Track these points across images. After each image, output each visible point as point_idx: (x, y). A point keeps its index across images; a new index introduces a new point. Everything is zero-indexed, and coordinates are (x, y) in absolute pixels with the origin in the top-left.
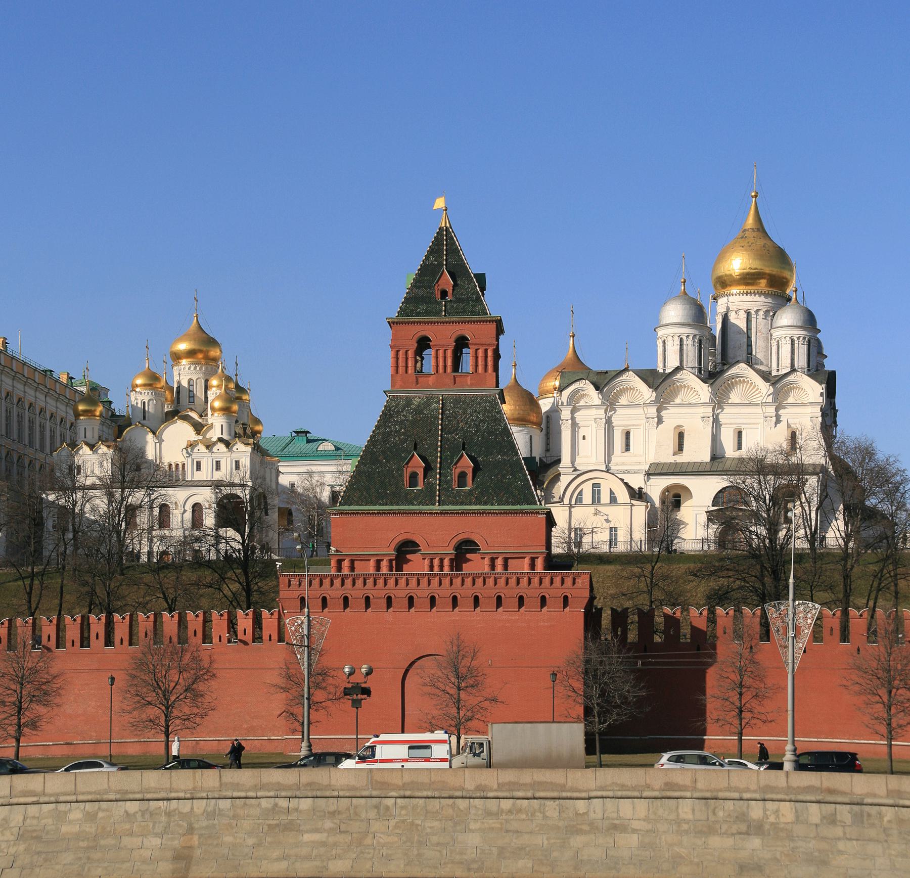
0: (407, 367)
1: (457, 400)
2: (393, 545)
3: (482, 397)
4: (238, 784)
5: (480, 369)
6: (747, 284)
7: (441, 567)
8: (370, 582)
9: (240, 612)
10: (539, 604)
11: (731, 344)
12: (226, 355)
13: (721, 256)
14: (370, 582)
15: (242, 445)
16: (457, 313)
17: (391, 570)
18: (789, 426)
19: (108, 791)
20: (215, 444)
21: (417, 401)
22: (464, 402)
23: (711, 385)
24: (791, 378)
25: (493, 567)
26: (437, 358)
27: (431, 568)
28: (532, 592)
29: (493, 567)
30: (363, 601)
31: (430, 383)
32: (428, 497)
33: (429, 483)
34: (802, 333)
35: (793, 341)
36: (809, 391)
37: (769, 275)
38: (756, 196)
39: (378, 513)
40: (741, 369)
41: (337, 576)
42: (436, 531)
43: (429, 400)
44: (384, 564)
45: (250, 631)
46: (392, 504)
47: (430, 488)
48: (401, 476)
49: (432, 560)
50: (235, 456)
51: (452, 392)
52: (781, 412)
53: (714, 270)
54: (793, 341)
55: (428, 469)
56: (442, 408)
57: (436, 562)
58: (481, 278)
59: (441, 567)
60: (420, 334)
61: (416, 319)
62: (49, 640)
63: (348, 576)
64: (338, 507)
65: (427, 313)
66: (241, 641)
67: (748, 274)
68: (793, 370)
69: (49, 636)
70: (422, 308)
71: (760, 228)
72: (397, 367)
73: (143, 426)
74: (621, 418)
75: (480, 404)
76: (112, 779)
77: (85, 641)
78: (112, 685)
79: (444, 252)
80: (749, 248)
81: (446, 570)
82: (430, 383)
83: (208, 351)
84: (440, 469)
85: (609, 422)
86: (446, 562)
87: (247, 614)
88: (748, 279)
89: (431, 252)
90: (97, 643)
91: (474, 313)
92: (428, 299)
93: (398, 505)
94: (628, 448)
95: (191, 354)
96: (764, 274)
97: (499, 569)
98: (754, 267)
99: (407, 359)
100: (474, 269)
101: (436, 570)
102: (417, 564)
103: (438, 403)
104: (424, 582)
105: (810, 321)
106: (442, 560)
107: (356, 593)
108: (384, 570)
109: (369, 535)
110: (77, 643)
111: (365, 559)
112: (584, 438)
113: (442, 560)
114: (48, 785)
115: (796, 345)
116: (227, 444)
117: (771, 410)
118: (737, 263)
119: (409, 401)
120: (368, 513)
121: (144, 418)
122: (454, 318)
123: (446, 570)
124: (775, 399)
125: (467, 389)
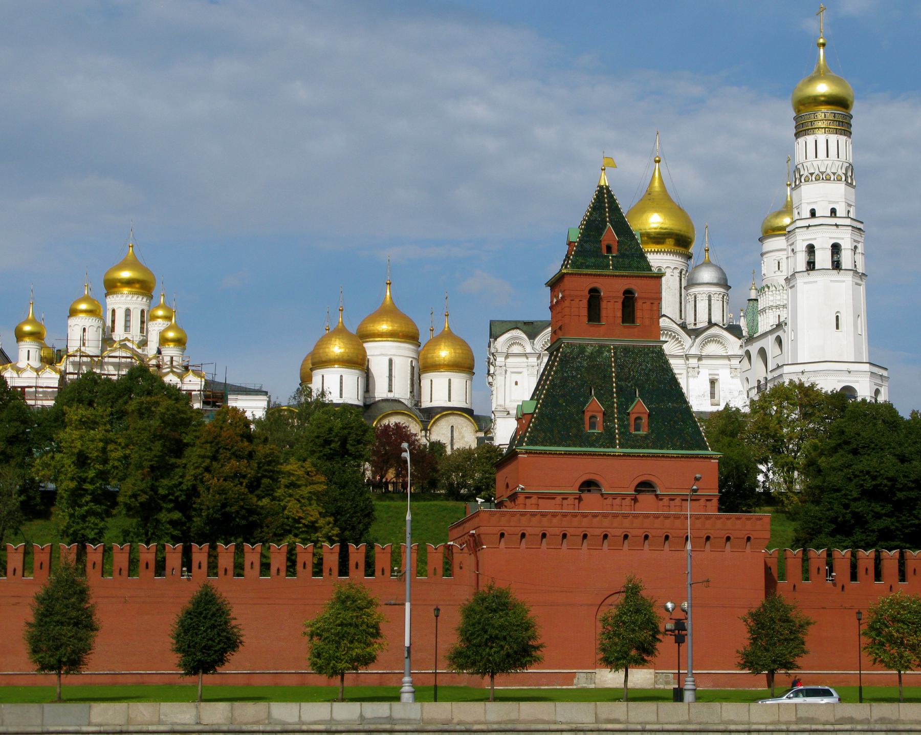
1: (626, 350)
4: (813, 719)
9: (195, 547)
16: (625, 268)
19: (689, 722)
21: (589, 350)
32: (608, 439)
33: (607, 426)
39: (624, 456)
42: (618, 470)
46: (575, 445)
47: (609, 432)
48: (582, 419)
54: (710, 297)
61: (589, 271)
64: (525, 446)
65: (597, 266)
68: (711, 324)
75: (648, 354)
76: (692, 710)
79: (605, 210)
90: (252, 573)
91: (638, 268)
92: (597, 254)
93: (581, 446)
98: (665, 226)
103: (609, 351)
114: (632, 714)
119: (582, 349)
120: (639, 456)
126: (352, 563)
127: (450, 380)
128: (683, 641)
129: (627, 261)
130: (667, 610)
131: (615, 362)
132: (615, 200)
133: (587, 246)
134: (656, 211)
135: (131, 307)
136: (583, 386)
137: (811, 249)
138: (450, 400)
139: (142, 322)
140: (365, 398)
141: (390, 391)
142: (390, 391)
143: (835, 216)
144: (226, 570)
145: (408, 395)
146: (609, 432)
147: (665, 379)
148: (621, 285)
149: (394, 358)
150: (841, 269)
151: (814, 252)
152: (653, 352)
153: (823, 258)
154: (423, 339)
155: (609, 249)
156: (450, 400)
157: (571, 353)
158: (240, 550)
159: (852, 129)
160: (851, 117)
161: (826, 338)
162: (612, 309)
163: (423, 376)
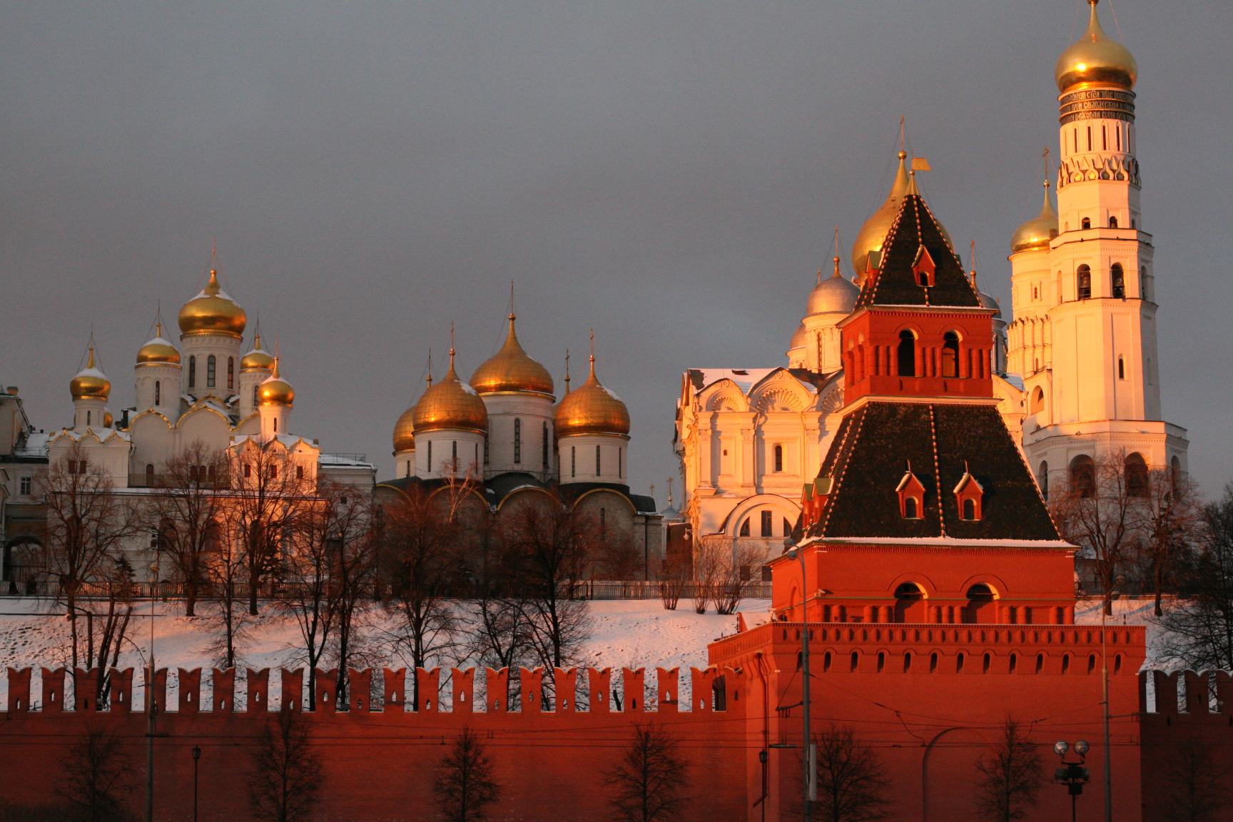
0: (889, 367)
2: (893, 589)
7: (951, 619)
10: (849, 664)
25: (1013, 618)
27: (939, 619)
29: (1013, 618)
31: (917, 388)
38: (904, 157)
44: (882, 612)
49: (939, 609)
55: (928, 498)
56: (934, 420)
57: (945, 611)
58: (958, 258)
59: (951, 619)
72: (877, 366)
74: (775, 429)
78: (196, 759)
82: (917, 388)
84: (942, 494)
85: (758, 432)
86: (957, 611)
94: (779, 466)
101: (945, 622)
102: (922, 615)
112: (725, 453)
113: (951, 609)
123: (957, 622)
127: (598, 447)
128: (1080, 792)
131: (936, 427)
132: (928, 215)
135: (216, 354)
137: (1084, 272)
138: (598, 474)
139: (231, 372)
141: (517, 462)
142: (517, 462)
143: (1116, 227)
145: (541, 468)
149: (522, 418)
150: (1124, 298)
151: (1089, 276)
153: (1100, 283)
154: (559, 393)
156: (598, 474)
159: (1136, 112)
160: (1134, 96)
163: (561, 441)
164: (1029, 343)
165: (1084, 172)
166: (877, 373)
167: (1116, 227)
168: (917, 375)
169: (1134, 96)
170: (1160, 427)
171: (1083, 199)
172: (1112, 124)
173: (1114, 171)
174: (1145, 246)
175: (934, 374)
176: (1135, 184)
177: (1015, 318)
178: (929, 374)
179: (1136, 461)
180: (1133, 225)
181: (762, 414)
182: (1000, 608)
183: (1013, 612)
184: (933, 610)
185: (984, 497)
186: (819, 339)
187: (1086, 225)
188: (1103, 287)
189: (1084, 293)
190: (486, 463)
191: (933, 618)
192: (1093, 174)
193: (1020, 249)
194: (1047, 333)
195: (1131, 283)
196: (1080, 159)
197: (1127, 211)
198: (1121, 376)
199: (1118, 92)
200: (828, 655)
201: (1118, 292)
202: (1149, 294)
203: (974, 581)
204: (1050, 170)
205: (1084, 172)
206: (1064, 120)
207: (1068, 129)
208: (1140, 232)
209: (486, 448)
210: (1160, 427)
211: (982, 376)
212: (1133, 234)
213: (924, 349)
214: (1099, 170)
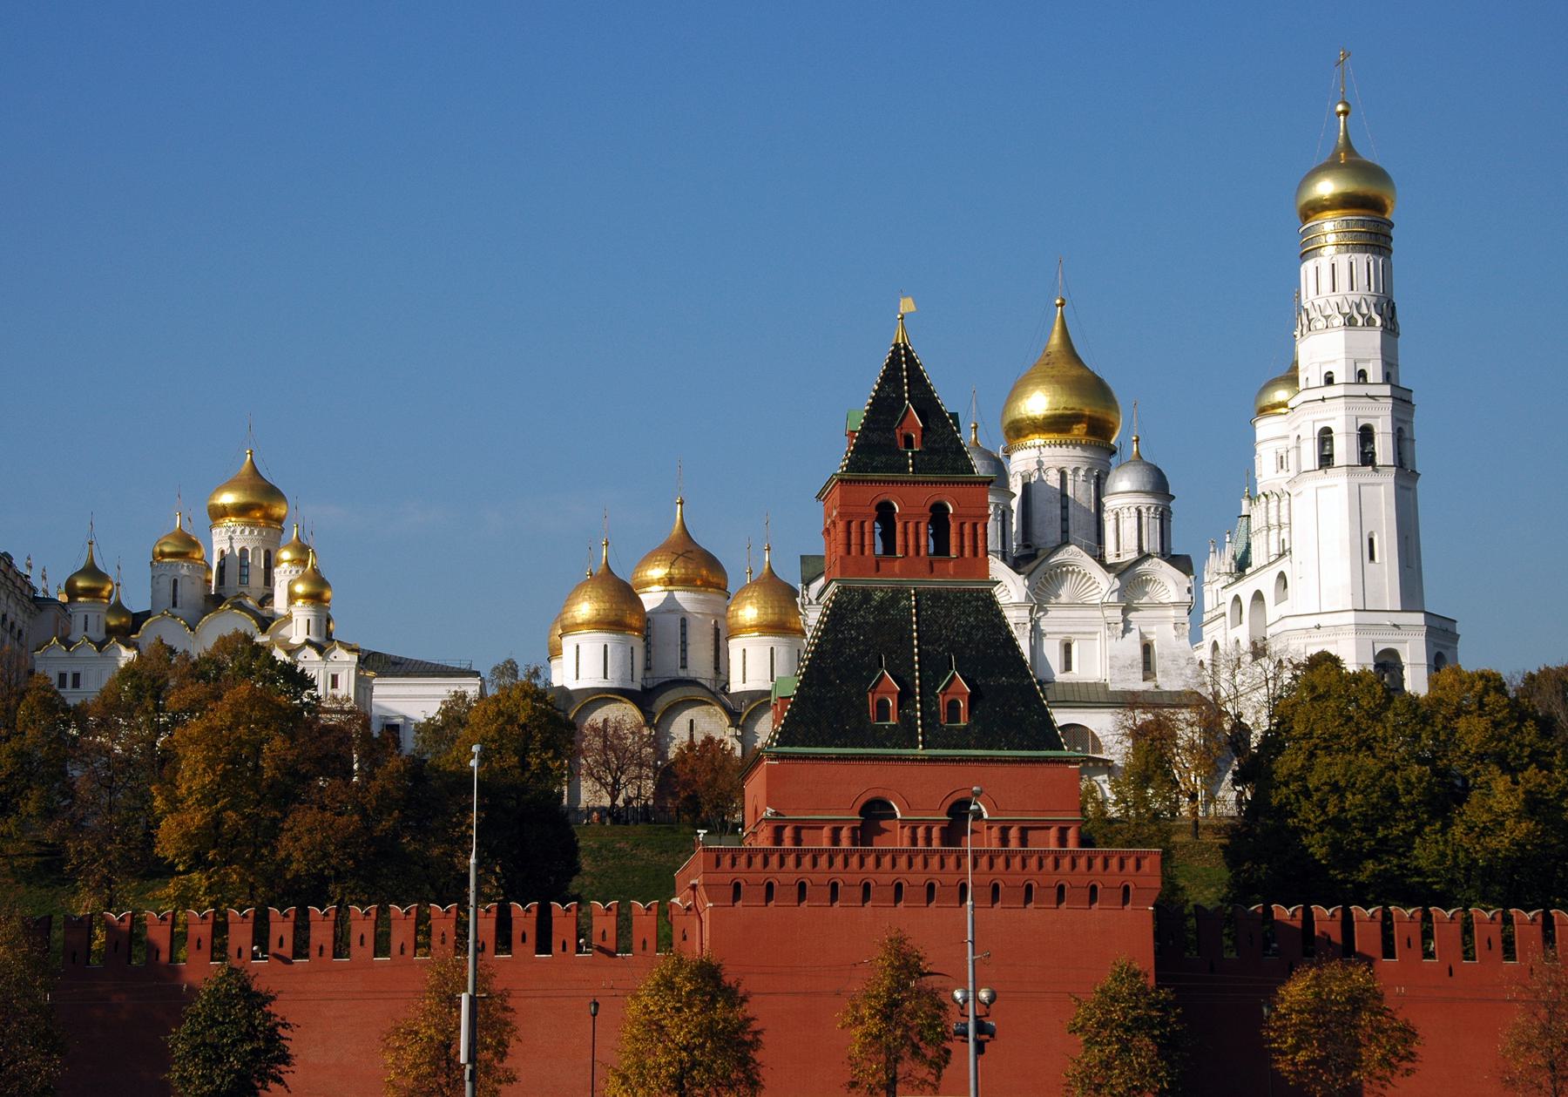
0: (863, 546)
1: (936, 596)
3: (971, 591)
5: (967, 552)
6: (1060, 431)
7: (928, 841)
8: (903, 862)
9: (517, 907)
10: (1055, 898)
11: (1036, 517)
12: (296, 513)
13: (1016, 391)
14: (903, 862)
15: (344, 652)
16: (932, 471)
17: (854, 844)
18: (1142, 636)
20: (301, 647)
22: (947, 599)
23: (1028, 576)
24: (1145, 567)
25: (1004, 840)
26: (849, 533)
27: (914, 841)
28: (1074, 880)
29: (1004, 840)
30: (828, 889)
31: (897, 569)
34: (1149, 501)
35: (1140, 513)
36: (1011, 587)
37: (1090, 418)
38: (1062, 305)
40: (1073, 554)
41: (772, 852)
42: (916, 786)
43: (898, 594)
44: (845, 833)
45: (611, 934)
47: (907, 721)
49: (914, 830)
50: (332, 668)
51: (936, 583)
52: (1132, 616)
53: (1004, 414)
54: (1140, 513)
55: (905, 697)
57: (921, 832)
58: (954, 416)
59: (928, 841)
60: (882, 498)
61: (876, 476)
62: (281, 945)
63: (789, 851)
65: (888, 468)
66: (276, 956)
67: (1061, 416)
69: (281, 939)
70: (879, 460)
71: (1069, 349)
72: (849, 545)
73: (174, 617)
77: (341, 946)
79: (903, 380)
80: (1059, 381)
81: (936, 845)
82: (897, 569)
83: (270, 506)
86: (936, 832)
87: (286, 915)
88: (1056, 425)
89: (886, 378)
90: (361, 952)
91: (955, 470)
92: (889, 448)
95: (241, 510)
96: (1083, 416)
97: (1014, 845)
99: (863, 534)
100: (948, 407)
101: (921, 846)
102: (896, 838)
103: (909, 599)
104: (823, 861)
105: (1159, 486)
106: (929, 831)
107: (817, 878)
108: (845, 844)
109: (839, 783)
110: (329, 951)
111: (817, 826)
113: (929, 831)
115: (1144, 520)
116: (321, 650)
117: (1117, 614)
118: (1038, 403)
119: (867, 595)
121: (175, 605)
122: (932, 477)
123: (936, 845)
124: (1121, 597)
125: (945, 580)
126: (354, 940)
129: (937, 459)
130: (955, 1001)
133: (875, 437)
134: (1037, 384)
136: (867, 652)
137: (1326, 436)
140: (644, 678)
141: (684, 667)
143: (1365, 382)
144: (321, 948)
146: (907, 721)
147: (996, 640)
148: (926, 496)
152: (977, 599)
155: (909, 442)
157: (850, 602)
158: (423, 920)
160: (1391, 225)
161: (1308, 576)
162: (915, 535)
164: (1273, 521)
165: (1327, 318)
166: (849, 552)
167: (1365, 382)
168: (953, 553)
169: (1391, 225)
170: (1419, 618)
171: (1325, 349)
172: (1361, 259)
173: (1363, 316)
174: (1402, 402)
175: (918, 553)
176: (1391, 329)
177: (1259, 492)
178: (911, 552)
179: (1391, 660)
180: (1387, 378)
181: (1041, 608)
182: (989, 828)
183: (1004, 832)
184: (906, 831)
185: (971, 697)
186: (1117, 520)
187: (1329, 380)
188: (1348, 452)
189: (1326, 460)
190: (647, 668)
191: (906, 840)
192: (1339, 320)
193: (1264, 411)
194: (1284, 512)
195: (1383, 448)
196: (1322, 302)
197: (1380, 362)
198: (1372, 557)
199: (1372, 225)
200: (770, 887)
201: (1367, 458)
202: (1407, 455)
203: (879, 793)
204: (1287, 314)
205: (1327, 318)
206: (1304, 256)
207: (1308, 268)
208: (1395, 387)
209: (648, 651)
210: (1419, 618)
211: (975, 553)
212: (1387, 390)
213: (906, 524)
214: (1344, 315)
